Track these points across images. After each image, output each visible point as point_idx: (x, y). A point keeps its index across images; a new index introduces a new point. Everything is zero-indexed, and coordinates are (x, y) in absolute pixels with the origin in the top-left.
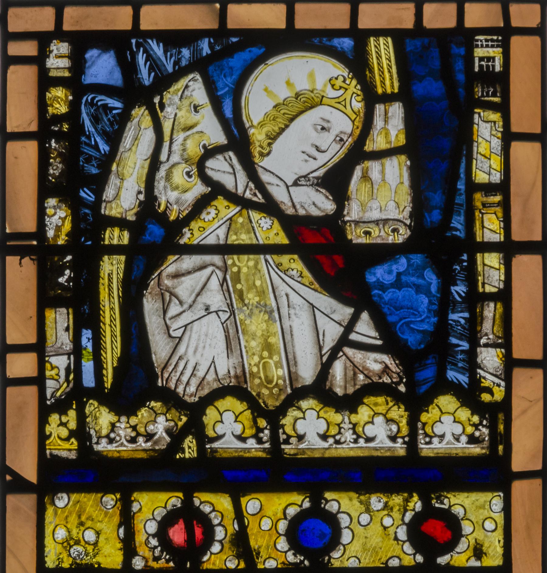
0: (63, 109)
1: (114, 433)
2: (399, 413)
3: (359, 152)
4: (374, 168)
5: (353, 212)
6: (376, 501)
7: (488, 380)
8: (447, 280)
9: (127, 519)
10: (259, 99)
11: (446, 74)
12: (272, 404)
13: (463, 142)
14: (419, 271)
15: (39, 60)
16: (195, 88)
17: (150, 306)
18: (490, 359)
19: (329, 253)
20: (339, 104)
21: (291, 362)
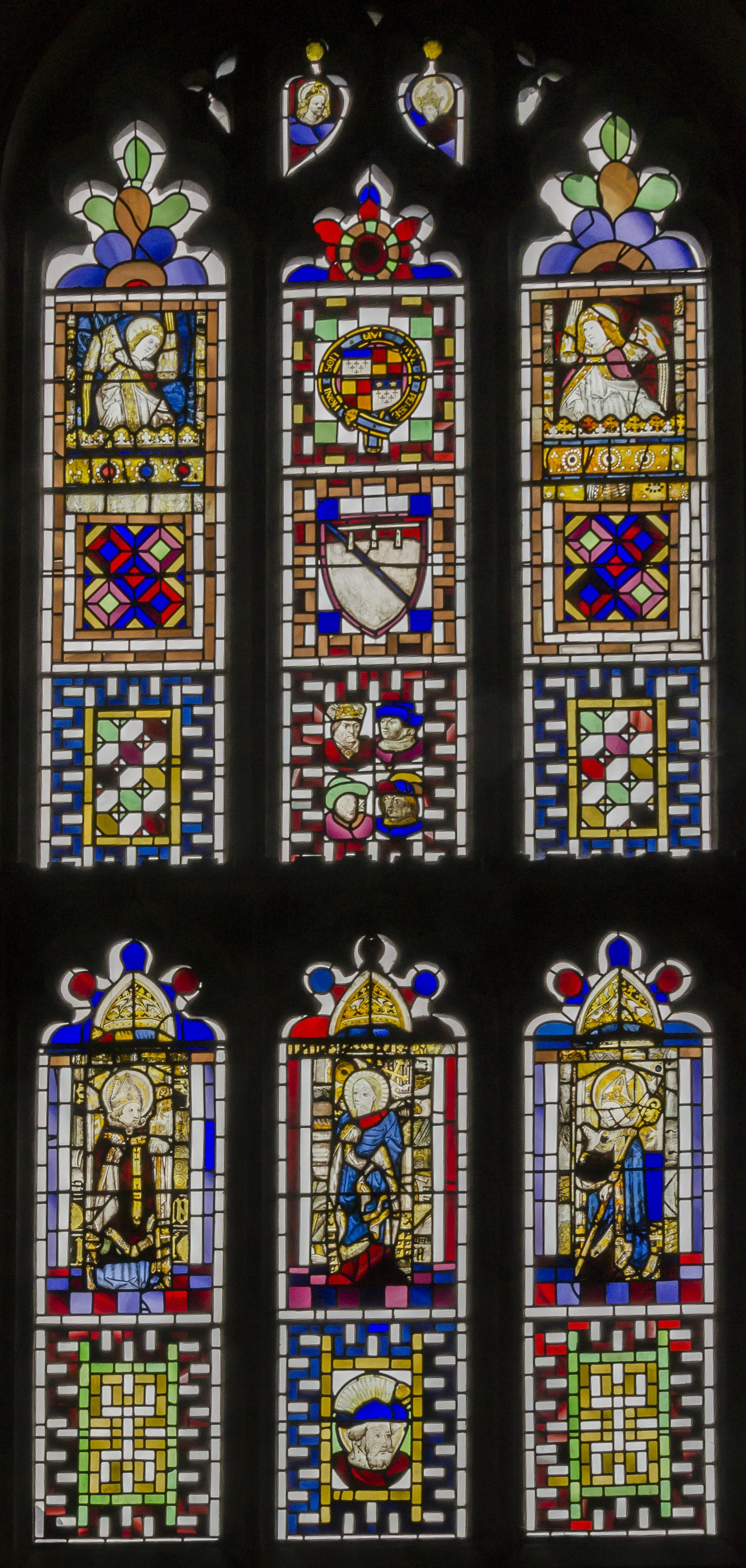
0: (72, 337)
1: (87, 440)
2: (173, 433)
3: (161, 350)
4: (166, 354)
5: (159, 369)
6: (165, 462)
7: (199, 422)
8: (188, 390)
9: (90, 467)
10: (132, 333)
11: (188, 324)
12: (135, 430)
13: (192, 346)
14: (179, 388)
15: (65, 321)
16: (113, 329)
17: (98, 399)
18: (200, 415)
19: (153, 382)
20: (156, 334)
21: (140, 417)
